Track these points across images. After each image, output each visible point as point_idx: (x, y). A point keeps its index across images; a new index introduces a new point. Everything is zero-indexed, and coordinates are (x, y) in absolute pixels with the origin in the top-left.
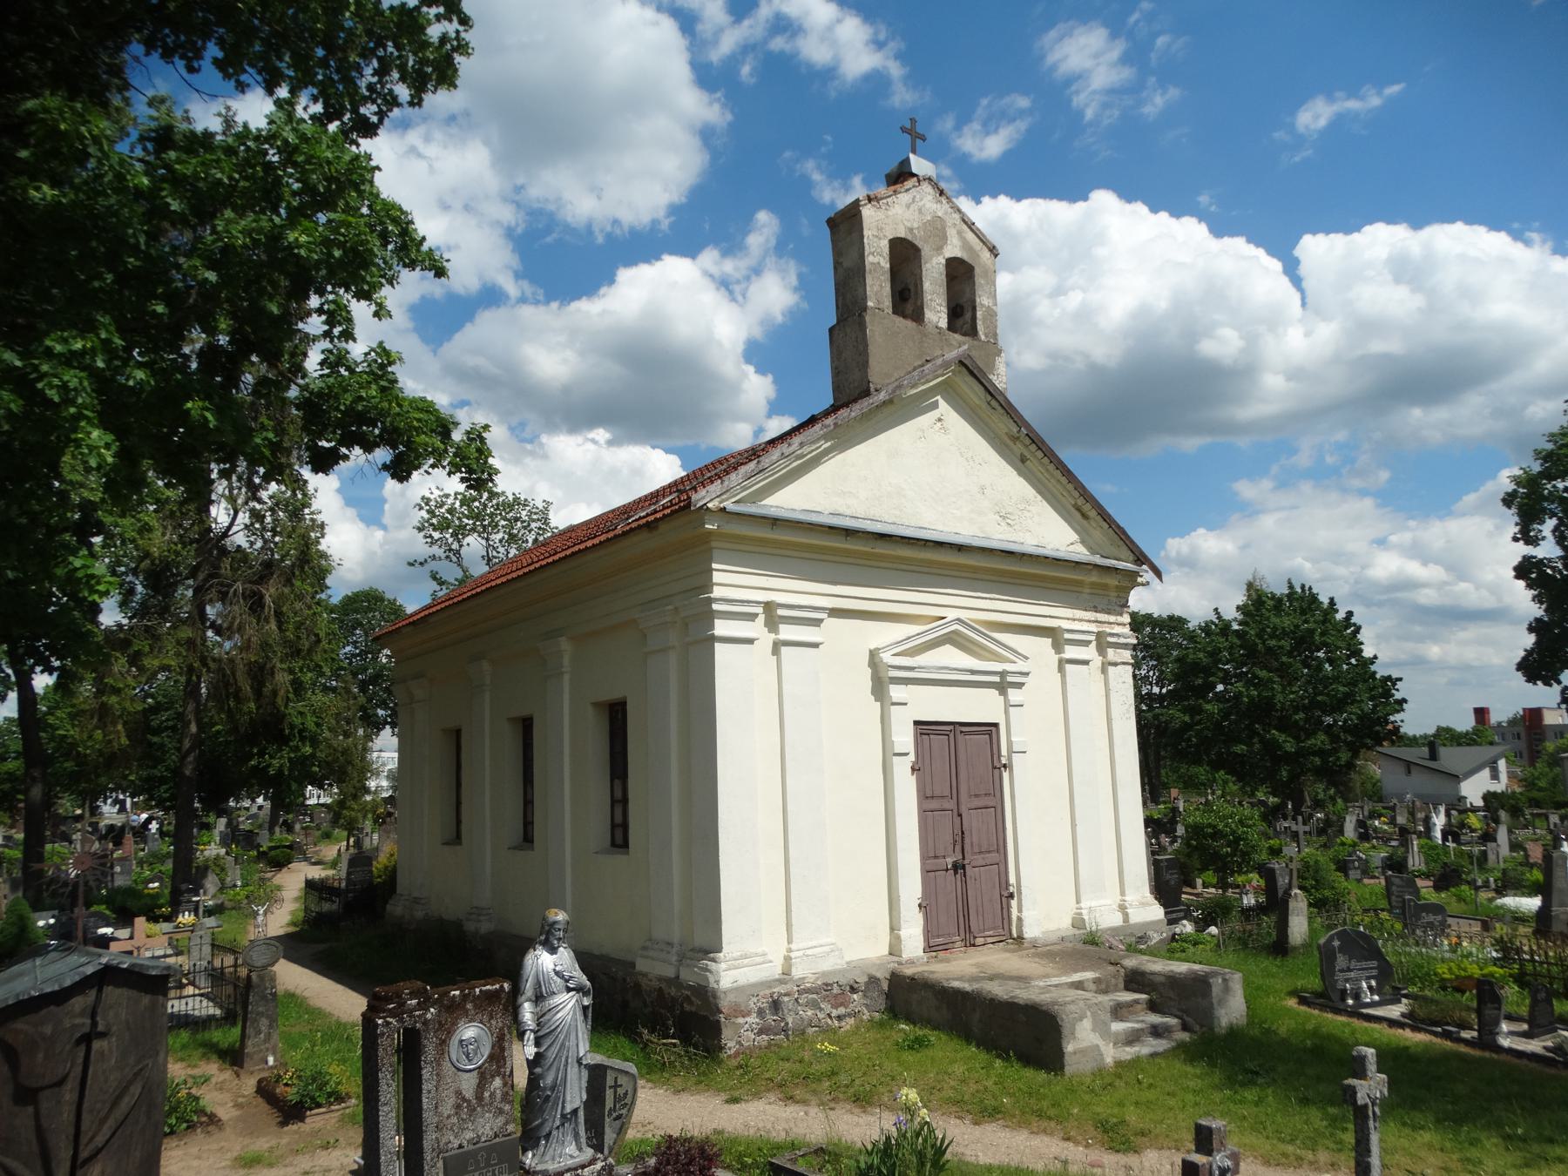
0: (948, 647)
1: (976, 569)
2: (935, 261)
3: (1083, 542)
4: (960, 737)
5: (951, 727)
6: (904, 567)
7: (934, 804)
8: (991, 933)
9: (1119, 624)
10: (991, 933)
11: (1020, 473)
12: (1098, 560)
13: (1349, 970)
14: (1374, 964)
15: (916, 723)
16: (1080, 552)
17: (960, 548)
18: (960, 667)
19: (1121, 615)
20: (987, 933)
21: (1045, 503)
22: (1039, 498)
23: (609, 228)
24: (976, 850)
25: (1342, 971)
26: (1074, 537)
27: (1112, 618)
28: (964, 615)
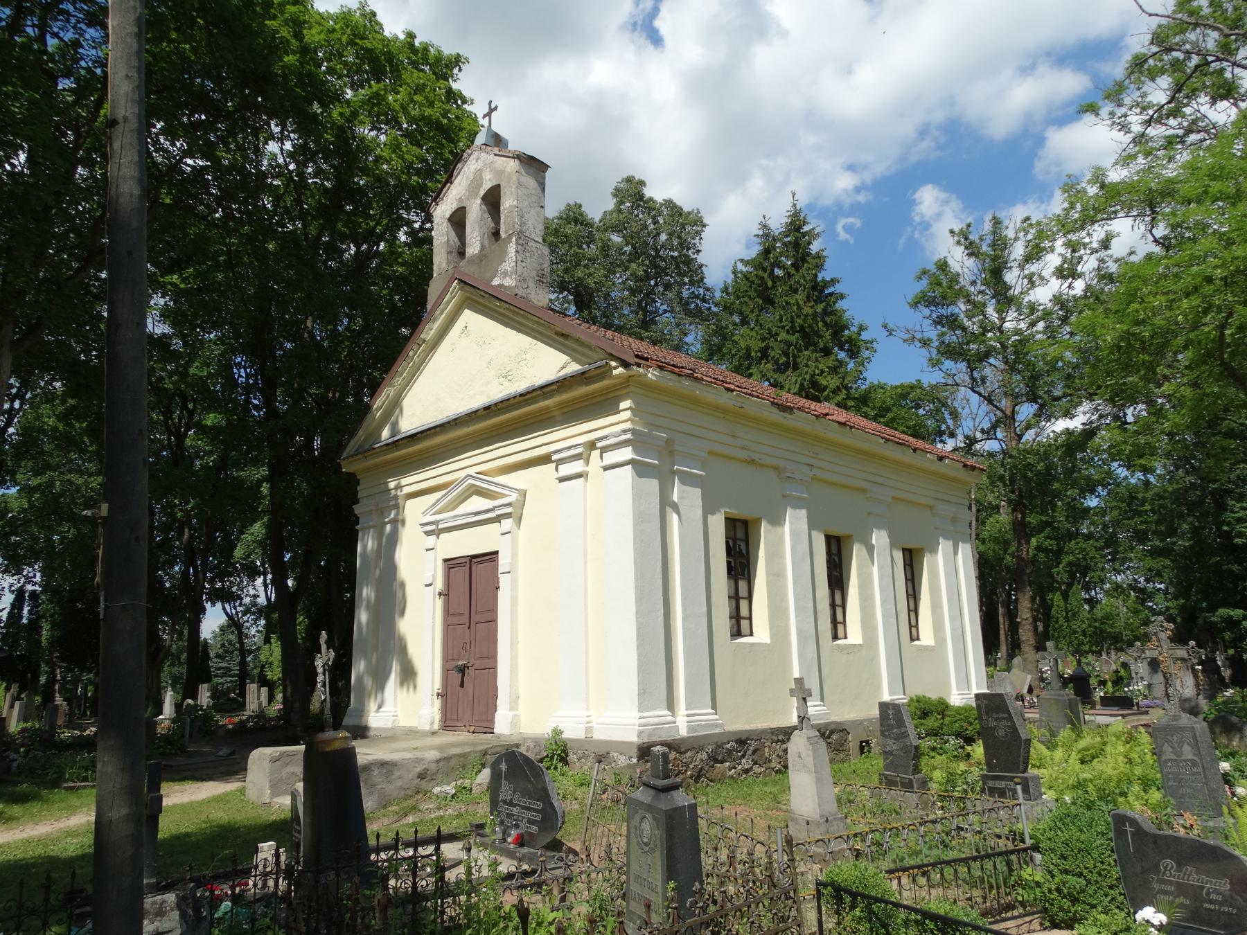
0: (474, 497)
3: (575, 360)
4: (474, 566)
13: (511, 804)
14: (539, 805)
15: (445, 561)
16: (574, 368)
21: (539, 343)
25: (505, 802)
26: (564, 358)
28: (472, 471)
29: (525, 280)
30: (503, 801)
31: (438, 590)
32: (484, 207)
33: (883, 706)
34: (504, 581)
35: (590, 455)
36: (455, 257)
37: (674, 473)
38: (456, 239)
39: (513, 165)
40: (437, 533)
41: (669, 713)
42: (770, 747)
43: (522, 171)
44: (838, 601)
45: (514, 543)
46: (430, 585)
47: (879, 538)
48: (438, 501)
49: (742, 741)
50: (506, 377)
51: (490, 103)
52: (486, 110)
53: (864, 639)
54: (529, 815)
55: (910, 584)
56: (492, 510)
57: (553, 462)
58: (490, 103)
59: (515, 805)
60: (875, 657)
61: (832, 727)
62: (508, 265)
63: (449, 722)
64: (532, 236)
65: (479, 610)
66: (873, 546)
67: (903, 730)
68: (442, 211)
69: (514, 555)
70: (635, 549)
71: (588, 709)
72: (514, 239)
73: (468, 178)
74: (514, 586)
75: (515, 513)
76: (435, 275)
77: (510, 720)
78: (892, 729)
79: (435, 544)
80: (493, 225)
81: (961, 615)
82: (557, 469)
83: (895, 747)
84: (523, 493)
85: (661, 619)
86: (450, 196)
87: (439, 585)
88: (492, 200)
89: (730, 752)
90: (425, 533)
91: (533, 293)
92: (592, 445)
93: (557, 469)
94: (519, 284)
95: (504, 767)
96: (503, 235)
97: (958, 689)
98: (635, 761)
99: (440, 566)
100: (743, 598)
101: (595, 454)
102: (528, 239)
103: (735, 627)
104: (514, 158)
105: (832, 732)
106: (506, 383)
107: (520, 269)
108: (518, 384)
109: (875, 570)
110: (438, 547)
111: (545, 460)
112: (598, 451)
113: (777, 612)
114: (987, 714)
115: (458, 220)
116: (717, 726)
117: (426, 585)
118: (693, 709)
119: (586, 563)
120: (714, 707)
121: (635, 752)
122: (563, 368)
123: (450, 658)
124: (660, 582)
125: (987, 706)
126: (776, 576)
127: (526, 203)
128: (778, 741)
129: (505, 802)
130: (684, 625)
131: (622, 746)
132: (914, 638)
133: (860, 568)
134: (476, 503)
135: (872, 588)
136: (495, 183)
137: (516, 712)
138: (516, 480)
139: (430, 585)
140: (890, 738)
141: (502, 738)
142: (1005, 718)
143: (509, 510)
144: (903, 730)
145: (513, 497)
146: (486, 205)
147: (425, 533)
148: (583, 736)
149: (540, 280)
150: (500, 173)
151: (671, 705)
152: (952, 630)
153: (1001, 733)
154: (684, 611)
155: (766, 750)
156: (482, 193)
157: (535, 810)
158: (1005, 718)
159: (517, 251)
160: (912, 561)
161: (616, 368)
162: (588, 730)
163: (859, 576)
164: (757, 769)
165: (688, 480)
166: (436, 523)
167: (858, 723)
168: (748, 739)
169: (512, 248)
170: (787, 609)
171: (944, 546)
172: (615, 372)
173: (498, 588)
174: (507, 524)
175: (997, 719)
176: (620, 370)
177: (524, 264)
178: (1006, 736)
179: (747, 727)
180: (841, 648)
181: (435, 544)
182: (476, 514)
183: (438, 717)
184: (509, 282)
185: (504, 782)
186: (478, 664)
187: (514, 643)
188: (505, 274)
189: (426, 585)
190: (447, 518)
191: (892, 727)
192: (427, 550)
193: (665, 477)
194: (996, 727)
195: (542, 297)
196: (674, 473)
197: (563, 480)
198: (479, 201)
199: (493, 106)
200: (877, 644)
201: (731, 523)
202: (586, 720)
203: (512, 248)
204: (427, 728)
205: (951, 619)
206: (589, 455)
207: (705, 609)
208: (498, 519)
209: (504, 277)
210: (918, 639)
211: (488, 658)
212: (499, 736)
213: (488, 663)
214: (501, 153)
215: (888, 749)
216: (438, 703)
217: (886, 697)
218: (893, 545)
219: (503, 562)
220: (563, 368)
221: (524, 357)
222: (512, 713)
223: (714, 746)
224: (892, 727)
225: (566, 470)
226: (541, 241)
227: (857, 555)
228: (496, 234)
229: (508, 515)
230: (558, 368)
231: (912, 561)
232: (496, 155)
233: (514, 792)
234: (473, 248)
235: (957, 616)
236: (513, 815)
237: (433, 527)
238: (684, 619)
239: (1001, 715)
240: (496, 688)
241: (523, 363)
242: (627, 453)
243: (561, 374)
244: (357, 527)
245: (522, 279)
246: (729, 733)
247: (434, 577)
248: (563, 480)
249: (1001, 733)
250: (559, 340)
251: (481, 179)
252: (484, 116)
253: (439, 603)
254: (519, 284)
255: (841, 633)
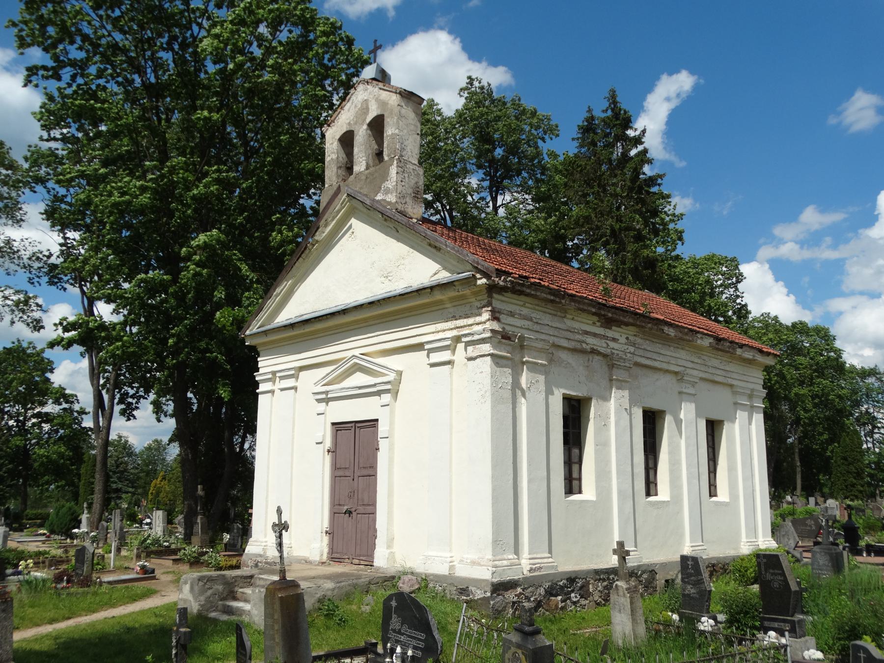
0: (358, 373)
1: (365, 320)
2: (361, 130)
3: (445, 268)
4: (357, 430)
5: (353, 425)
6: (343, 330)
7: (340, 473)
8: (363, 558)
9: (478, 324)
10: (363, 558)
11: (398, 240)
12: (456, 277)
13: (399, 632)
14: (422, 636)
15: (333, 424)
16: (444, 276)
17: (344, 312)
18: (351, 386)
19: (480, 315)
20: (361, 558)
21: (415, 252)
22: (412, 250)
23: (25, 345)
24: (360, 503)
25: (394, 631)
26: (437, 266)
27: (470, 321)
28: (357, 352)
29: (404, 197)
30: (392, 629)
31: (327, 448)
32: (369, 132)
33: (684, 558)
34: (383, 444)
35: (456, 346)
36: (342, 172)
37: (523, 363)
38: (344, 156)
39: (394, 99)
40: (327, 401)
41: (516, 557)
42: (593, 584)
43: (403, 104)
44: (651, 465)
45: (392, 413)
46: (321, 443)
47: (687, 411)
48: (328, 374)
49: (572, 579)
50: (387, 277)
51: (376, 41)
52: (372, 48)
53: (672, 497)
54: (414, 642)
55: (711, 463)
56: (375, 385)
57: (425, 350)
58: (376, 41)
59: (403, 634)
60: (680, 511)
61: (644, 568)
62: (390, 184)
63: (335, 556)
64: (410, 160)
65: (361, 466)
66: (681, 420)
67: (700, 577)
68: (332, 135)
69: (392, 423)
70: (492, 426)
71: (450, 551)
72: (395, 162)
73: (356, 106)
74: (391, 448)
75: (393, 389)
76: (326, 186)
77: (387, 556)
78: (691, 576)
79: (325, 410)
80: (376, 147)
81: (752, 475)
82: (428, 356)
83: (693, 591)
84: (400, 373)
85: (511, 482)
86: (340, 120)
87: (328, 444)
88: (377, 126)
89: (562, 588)
90: (317, 400)
91: (410, 207)
92: (457, 339)
93: (428, 356)
94: (398, 200)
95: (394, 603)
96: (386, 158)
97: (747, 537)
98: (489, 594)
99: (329, 428)
100: (575, 463)
101: (460, 346)
102: (406, 162)
103: (568, 485)
104: (396, 93)
105: (643, 572)
106: (387, 282)
107: (400, 188)
108: (397, 284)
109: (683, 443)
110: (327, 413)
111: (419, 347)
112: (463, 344)
113: (602, 475)
114: (766, 571)
115: (347, 140)
116: (553, 567)
117: (317, 443)
118: (536, 553)
119: (451, 434)
120: (550, 552)
121: (489, 588)
122: (435, 274)
123: (337, 502)
124: (511, 452)
125: (765, 564)
126: (603, 445)
127: (405, 131)
128: (600, 579)
129: (394, 631)
130: (528, 487)
131: (477, 582)
132: (713, 492)
133: (670, 438)
134: (359, 379)
135: (680, 455)
136: (379, 113)
137: (391, 550)
138: (395, 362)
139: (321, 443)
140: (689, 584)
141: (381, 571)
142: (779, 574)
143: (388, 387)
144: (700, 577)
145: (392, 377)
146: (371, 130)
147: (317, 400)
148: (447, 573)
149: (416, 196)
150: (383, 104)
151: (517, 552)
152: (744, 488)
153: (776, 585)
154: (529, 474)
155: (591, 586)
156: (369, 119)
157: (419, 640)
158: (779, 574)
159: (397, 173)
160: (713, 428)
161: (480, 279)
162: (452, 567)
163: (670, 444)
164: (583, 602)
165: (534, 368)
166: (327, 393)
167: (664, 565)
168: (576, 578)
169: (393, 170)
170: (610, 472)
171: (742, 416)
172: (479, 282)
173: (378, 449)
174: (386, 398)
175: (772, 574)
176: (484, 281)
177: (403, 183)
178: (780, 588)
179: (577, 568)
180: (650, 502)
181: (325, 410)
182: (360, 388)
183: (326, 550)
184: (392, 198)
185: (394, 616)
186: (361, 509)
187: (390, 494)
188: (387, 191)
189: (317, 443)
190: (335, 389)
191: (691, 575)
192: (318, 414)
193: (516, 367)
194: (772, 580)
195: (417, 211)
196: (523, 363)
197: (433, 365)
198: (365, 127)
199: (378, 45)
200: (682, 500)
201: (567, 399)
202: (449, 560)
203: (393, 170)
204: (317, 559)
205: (744, 480)
206: (456, 347)
207: (545, 473)
208: (378, 393)
209: (386, 194)
210: (716, 495)
211: (369, 505)
212: (379, 568)
213: (369, 509)
214: (385, 88)
215: (687, 592)
216: (326, 539)
217: (687, 551)
218: (698, 415)
219: (383, 429)
220: (435, 274)
221: (403, 262)
222: (389, 551)
223: (550, 584)
224: (691, 575)
225: (436, 357)
226: (416, 162)
227: (668, 425)
228: (379, 155)
229: (387, 391)
230: (431, 274)
231: (713, 428)
232: (380, 89)
233: (402, 624)
234: (360, 166)
235: (749, 477)
236: (401, 641)
237: (324, 396)
238: (529, 481)
239: (776, 571)
240: (376, 531)
241: (401, 267)
242: (487, 348)
243: (433, 279)
244: (257, 391)
245: (401, 196)
246: (562, 573)
247: (324, 436)
248: (433, 365)
249: (776, 585)
250: (432, 249)
251: (367, 109)
252: (370, 53)
253: (328, 458)
254: (398, 200)
255: (652, 492)
